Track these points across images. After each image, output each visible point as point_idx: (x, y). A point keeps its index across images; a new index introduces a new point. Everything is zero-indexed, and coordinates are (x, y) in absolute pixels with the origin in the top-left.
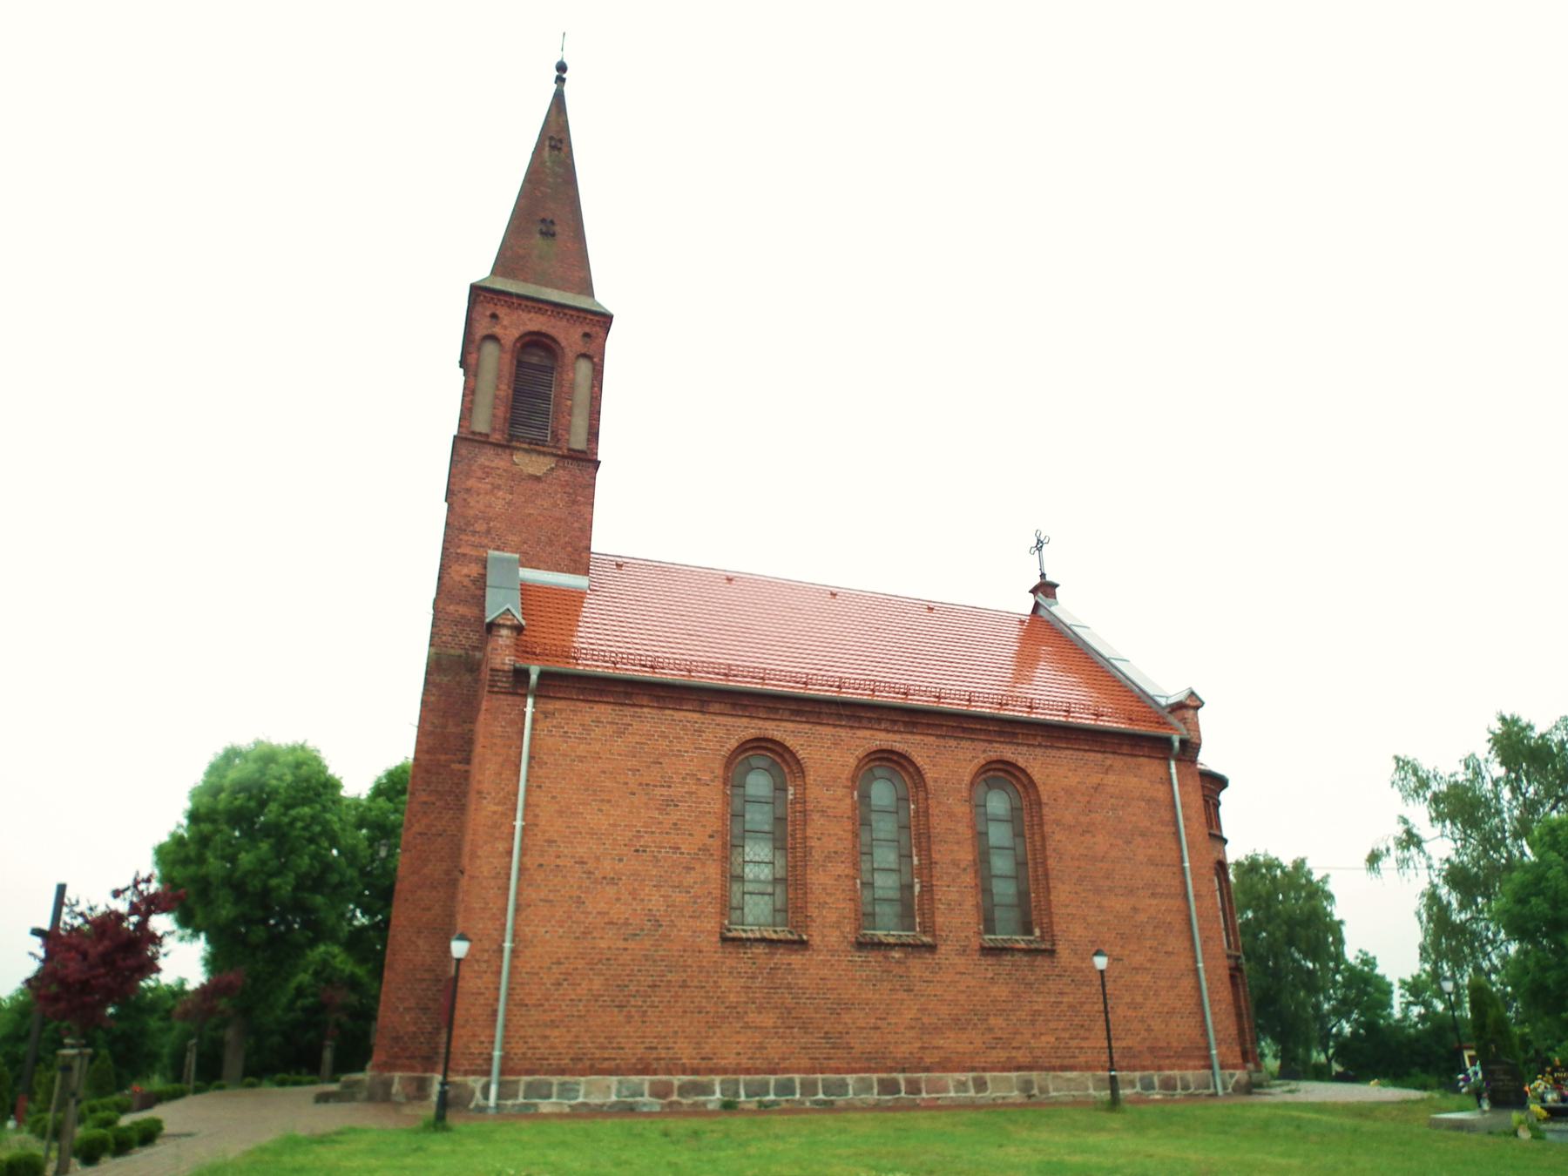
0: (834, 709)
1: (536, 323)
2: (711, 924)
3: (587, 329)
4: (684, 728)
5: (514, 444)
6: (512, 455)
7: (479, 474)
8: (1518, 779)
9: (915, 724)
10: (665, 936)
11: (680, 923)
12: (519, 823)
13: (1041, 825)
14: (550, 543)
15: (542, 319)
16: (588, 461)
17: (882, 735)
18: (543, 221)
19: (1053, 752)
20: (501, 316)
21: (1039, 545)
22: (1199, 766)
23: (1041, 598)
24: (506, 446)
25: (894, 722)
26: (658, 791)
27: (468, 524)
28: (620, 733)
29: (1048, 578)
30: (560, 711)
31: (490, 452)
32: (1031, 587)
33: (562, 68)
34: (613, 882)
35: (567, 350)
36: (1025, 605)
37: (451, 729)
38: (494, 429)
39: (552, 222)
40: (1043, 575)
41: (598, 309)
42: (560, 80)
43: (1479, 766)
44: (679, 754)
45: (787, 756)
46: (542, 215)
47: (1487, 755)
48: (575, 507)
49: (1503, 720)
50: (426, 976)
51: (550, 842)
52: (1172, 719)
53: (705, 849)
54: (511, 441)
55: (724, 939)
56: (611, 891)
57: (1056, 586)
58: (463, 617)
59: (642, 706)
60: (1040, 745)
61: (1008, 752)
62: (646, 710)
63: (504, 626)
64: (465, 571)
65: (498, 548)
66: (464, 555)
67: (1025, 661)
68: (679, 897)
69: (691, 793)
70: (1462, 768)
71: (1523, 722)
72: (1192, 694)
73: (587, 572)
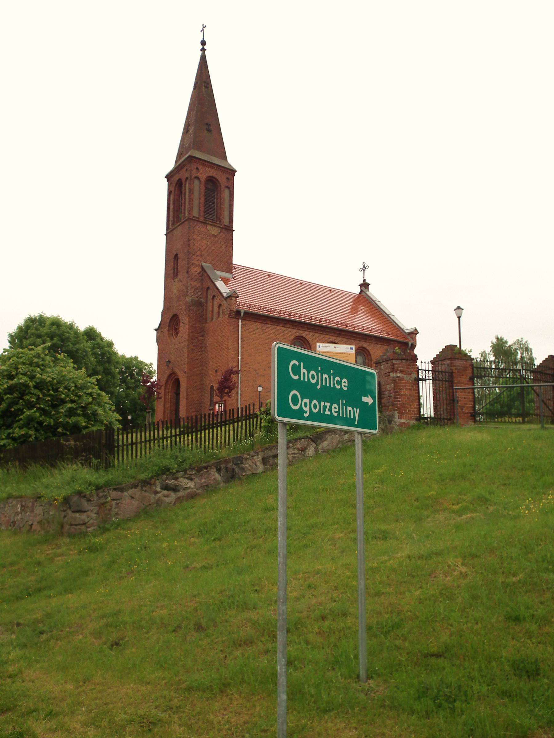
1: (211, 172)
3: (227, 176)
5: (207, 222)
7: (197, 233)
8: (498, 362)
12: (240, 358)
16: (229, 229)
17: (332, 337)
18: (207, 124)
19: (377, 346)
20: (200, 169)
21: (364, 269)
22: (353, 347)
23: (363, 289)
25: (335, 333)
29: (366, 281)
31: (200, 224)
32: (359, 284)
33: (203, 43)
34: (263, 376)
35: (222, 185)
36: (357, 290)
38: (199, 215)
39: (210, 125)
40: (364, 280)
42: (203, 50)
43: (486, 356)
45: (306, 342)
47: (489, 352)
49: (497, 338)
50: (197, 402)
51: (247, 364)
52: (409, 337)
54: (206, 221)
58: (196, 286)
62: (270, 325)
63: (233, 296)
66: (194, 264)
67: (354, 310)
70: (480, 356)
71: (505, 339)
72: (416, 330)
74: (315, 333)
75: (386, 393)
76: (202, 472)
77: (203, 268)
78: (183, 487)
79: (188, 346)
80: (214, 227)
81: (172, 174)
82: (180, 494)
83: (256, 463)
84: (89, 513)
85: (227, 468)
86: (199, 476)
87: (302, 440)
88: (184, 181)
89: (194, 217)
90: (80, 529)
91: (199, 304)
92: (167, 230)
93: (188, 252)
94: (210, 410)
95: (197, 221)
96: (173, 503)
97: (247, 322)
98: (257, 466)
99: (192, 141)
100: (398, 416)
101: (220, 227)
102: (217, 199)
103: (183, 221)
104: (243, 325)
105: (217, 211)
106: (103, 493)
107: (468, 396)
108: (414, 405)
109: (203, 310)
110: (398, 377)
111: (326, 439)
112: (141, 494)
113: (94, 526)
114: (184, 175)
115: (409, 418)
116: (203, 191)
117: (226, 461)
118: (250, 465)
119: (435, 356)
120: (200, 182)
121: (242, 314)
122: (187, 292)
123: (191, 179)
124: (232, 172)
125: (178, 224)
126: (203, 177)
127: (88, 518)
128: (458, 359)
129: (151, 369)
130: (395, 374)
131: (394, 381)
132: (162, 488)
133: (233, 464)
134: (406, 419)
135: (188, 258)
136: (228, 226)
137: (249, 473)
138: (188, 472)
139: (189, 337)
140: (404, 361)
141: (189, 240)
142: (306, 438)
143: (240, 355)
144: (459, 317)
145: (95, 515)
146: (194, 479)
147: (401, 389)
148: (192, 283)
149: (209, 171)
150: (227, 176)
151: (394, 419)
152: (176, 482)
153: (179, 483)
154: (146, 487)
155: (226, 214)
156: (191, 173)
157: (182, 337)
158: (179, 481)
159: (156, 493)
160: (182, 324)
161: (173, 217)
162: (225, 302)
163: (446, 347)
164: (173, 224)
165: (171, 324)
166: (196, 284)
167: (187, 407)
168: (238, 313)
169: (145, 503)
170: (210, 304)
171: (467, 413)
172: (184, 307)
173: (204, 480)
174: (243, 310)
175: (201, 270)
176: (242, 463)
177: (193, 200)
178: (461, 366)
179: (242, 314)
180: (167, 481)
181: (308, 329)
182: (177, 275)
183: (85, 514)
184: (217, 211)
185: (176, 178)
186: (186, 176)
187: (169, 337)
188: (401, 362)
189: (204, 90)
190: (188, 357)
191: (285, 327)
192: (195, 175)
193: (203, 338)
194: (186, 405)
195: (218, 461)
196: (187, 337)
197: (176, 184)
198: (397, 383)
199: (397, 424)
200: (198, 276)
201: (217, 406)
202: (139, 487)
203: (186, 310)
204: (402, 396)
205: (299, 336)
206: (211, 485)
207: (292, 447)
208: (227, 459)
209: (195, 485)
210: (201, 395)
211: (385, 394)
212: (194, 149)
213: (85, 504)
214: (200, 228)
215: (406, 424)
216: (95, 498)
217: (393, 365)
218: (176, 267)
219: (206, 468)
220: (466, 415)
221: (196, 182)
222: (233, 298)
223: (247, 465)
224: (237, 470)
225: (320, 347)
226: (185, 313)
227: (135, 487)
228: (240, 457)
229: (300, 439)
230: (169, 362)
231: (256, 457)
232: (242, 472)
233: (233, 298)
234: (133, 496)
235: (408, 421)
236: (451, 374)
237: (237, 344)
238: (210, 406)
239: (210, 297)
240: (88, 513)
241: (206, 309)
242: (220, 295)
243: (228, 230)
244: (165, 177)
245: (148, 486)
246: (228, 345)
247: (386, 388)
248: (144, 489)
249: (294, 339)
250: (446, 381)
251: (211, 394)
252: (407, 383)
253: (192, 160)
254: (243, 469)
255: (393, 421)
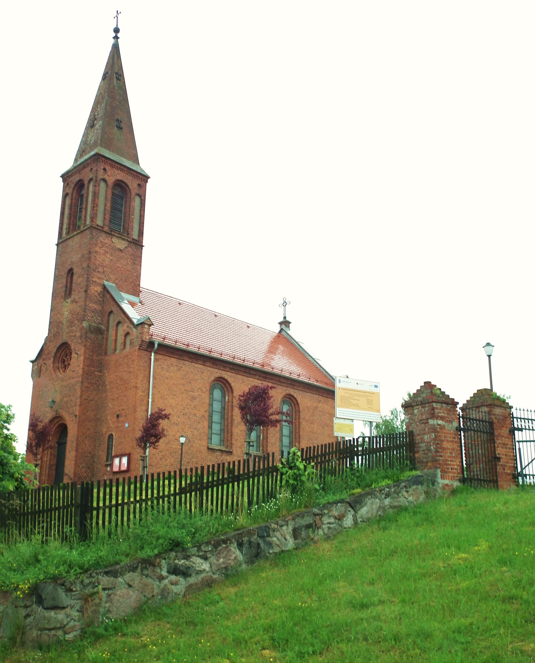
0: (243, 369)
1: (120, 176)
2: (204, 443)
3: (139, 182)
4: (198, 371)
6: (112, 238)
7: (100, 245)
9: (266, 378)
10: (192, 446)
11: (196, 442)
12: (150, 400)
13: (299, 419)
14: (126, 281)
15: (123, 174)
16: (138, 244)
17: (256, 381)
18: (118, 120)
19: (305, 393)
21: (285, 304)
23: (284, 327)
24: (110, 234)
25: (260, 376)
26: (191, 393)
27: (96, 268)
28: (179, 370)
29: (287, 319)
30: (161, 359)
32: (279, 321)
33: (117, 30)
34: (177, 425)
35: (132, 191)
36: (277, 329)
37: (95, 357)
40: (285, 318)
41: (143, 173)
42: (116, 38)
44: (196, 380)
45: (227, 385)
46: (117, 118)
48: (135, 266)
53: (203, 416)
54: (111, 231)
55: (209, 449)
56: (176, 428)
57: (290, 323)
58: (95, 309)
59: (186, 361)
60: (301, 390)
61: (292, 392)
62: (186, 362)
64: (96, 289)
65: (107, 281)
66: (95, 282)
67: (272, 349)
68: (196, 432)
69: (200, 395)
73: (138, 296)
74: (239, 374)
75: (423, 445)
76: (220, 548)
77: (104, 287)
78: (195, 570)
79: (82, 382)
80: (120, 241)
81: (70, 174)
82: (192, 580)
83: (285, 536)
84: (68, 610)
85: (250, 542)
86: (216, 555)
87: (339, 504)
88: (86, 183)
89: (98, 225)
90: (55, 635)
91: (98, 331)
92: (58, 239)
93: (88, 267)
94: (107, 466)
95: (101, 231)
96: (183, 593)
97: (160, 357)
98: (286, 540)
99: (100, 137)
100: (441, 475)
101: (128, 241)
102: (125, 208)
103: (82, 229)
104: (156, 360)
105: (124, 222)
106: (90, 580)
107: (509, 452)
108: (456, 462)
109: (103, 338)
110: (439, 425)
111: (366, 504)
112: (141, 579)
113: (76, 631)
114: (86, 175)
115: (453, 478)
116: (110, 196)
117: (250, 533)
118: (278, 539)
119: (465, 402)
120: (107, 185)
121: (156, 346)
122: (84, 316)
123: (96, 181)
124: (145, 179)
125: (75, 233)
126: (111, 180)
127: (67, 617)
128: (497, 406)
129: (9, 412)
130: (435, 420)
131: (434, 429)
132: (169, 572)
133: (258, 536)
134: (449, 479)
135: (88, 274)
136: (136, 240)
137: (277, 550)
138: (203, 548)
139: (84, 371)
140: (444, 405)
141: (90, 252)
142: (342, 501)
143: (150, 397)
144: (489, 356)
145: (77, 614)
146: (210, 557)
147: (442, 441)
148: (91, 305)
149: (118, 174)
150: (139, 182)
151: (436, 479)
152: (187, 563)
153: (191, 564)
154: (147, 569)
155: (136, 226)
156: (97, 174)
157: (74, 371)
158: (191, 561)
159: (161, 578)
160: (74, 355)
161: (69, 224)
162: (134, 330)
163: (478, 391)
164: (68, 233)
165: (58, 354)
166: (95, 306)
167: (76, 461)
168: (151, 344)
169: (146, 594)
170: (112, 332)
171: (509, 475)
172: (78, 334)
173: (221, 560)
174: (157, 340)
175: (102, 290)
176: (269, 536)
177: (97, 206)
178: (501, 415)
179: (156, 346)
180: (176, 561)
181: (231, 369)
182: (70, 294)
183: (63, 612)
184: (124, 222)
185: (76, 178)
186: (91, 177)
187: (54, 371)
188: (442, 406)
189: (115, 82)
190: (81, 397)
191: (204, 365)
192: (102, 177)
193: (101, 374)
194: (74, 459)
195: (239, 532)
196: (81, 371)
197: (75, 186)
198: (438, 432)
199: (440, 485)
200: (98, 297)
201: (117, 461)
202: (139, 570)
203: (81, 337)
204: (443, 450)
205: (220, 378)
206: (231, 567)
207: (328, 513)
208: (250, 530)
209: (211, 567)
210: (95, 447)
211: (421, 447)
212: (101, 146)
213: (63, 598)
214: (103, 238)
215: (449, 486)
216: (78, 587)
217: (433, 409)
218: (69, 284)
219: (225, 542)
220: (509, 477)
221: (102, 185)
222: (146, 326)
223: (275, 539)
224: (262, 545)
225: (340, 382)
226: (80, 341)
227: (133, 569)
228: (266, 526)
229: (336, 503)
230: (53, 402)
231: (284, 528)
232: (269, 549)
233: (146, 326)
234: (130, 583)
235: (452, 482)
236: (491, 423)
237: (147, 383)
238: (107, 460)
239: (112, 323)
240: (67, 610)
241: (107, 339)
242: (128, 321)
243: (138, 245)
244: (62, 176)
245: (150, 569)
246: (136, 383)
247: (421, 439)
248: (145, 572)
249: (214, 380)
250: (484, 432)
251: (108, 445)
252: (448, 433)
253: (99, 158)
254: (270, 545)
255: (436, 481)
